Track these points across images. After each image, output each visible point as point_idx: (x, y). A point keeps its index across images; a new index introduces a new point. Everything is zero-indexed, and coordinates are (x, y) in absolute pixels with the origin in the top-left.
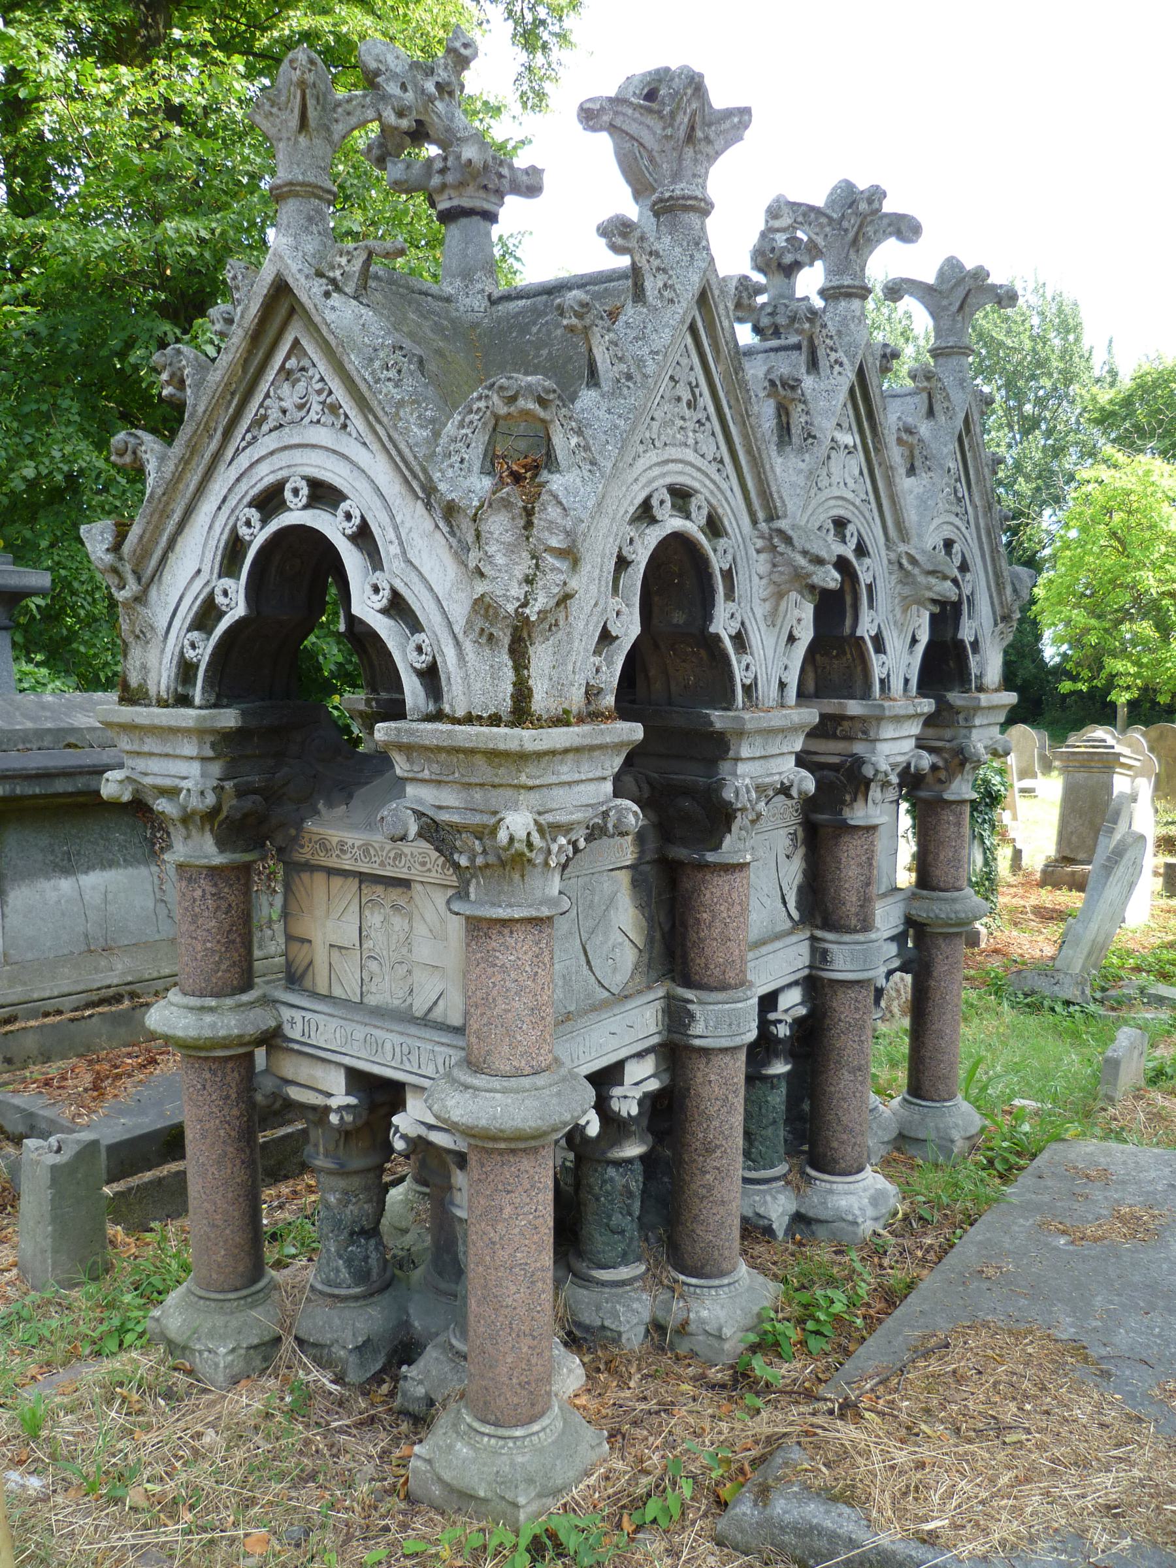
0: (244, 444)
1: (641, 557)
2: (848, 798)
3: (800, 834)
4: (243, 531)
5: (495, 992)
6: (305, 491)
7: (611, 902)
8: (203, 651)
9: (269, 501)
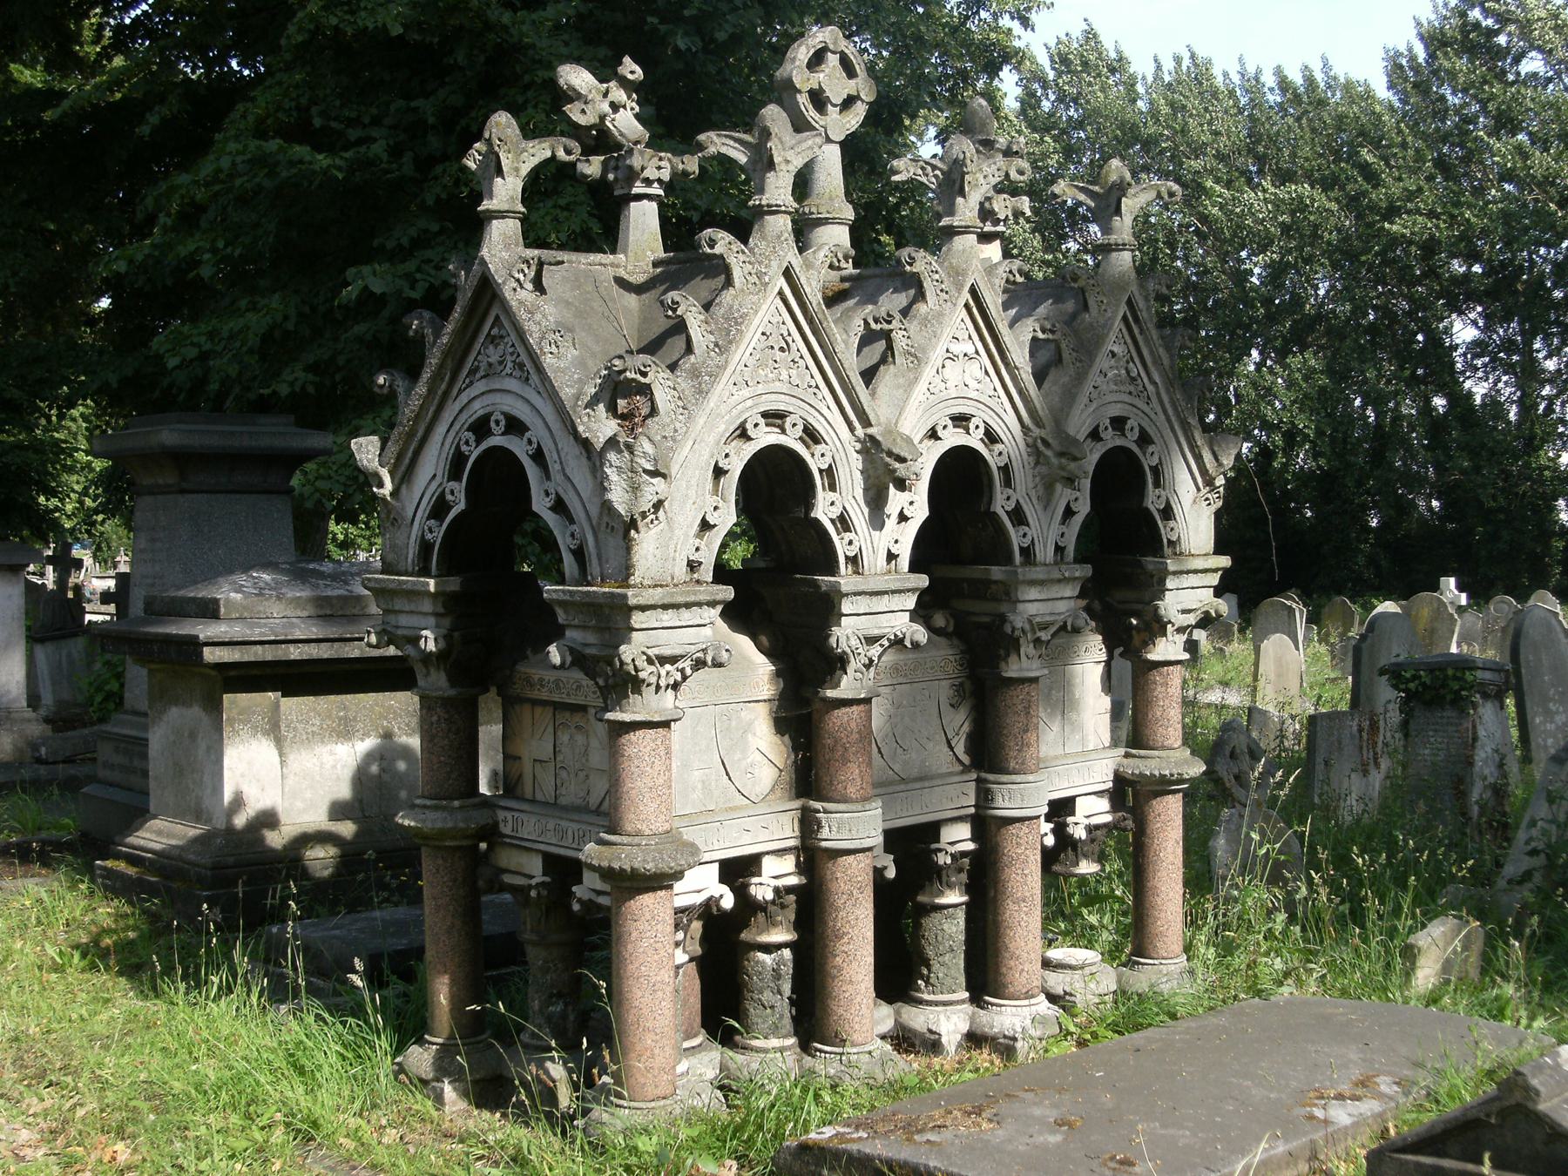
1: (736, 467)
2: (1002, 652)
3: (968, 686)
4: (464, 448)
6: (503, 423)
7: (748, 728)
8: (438, 534)
9: (481, 428)
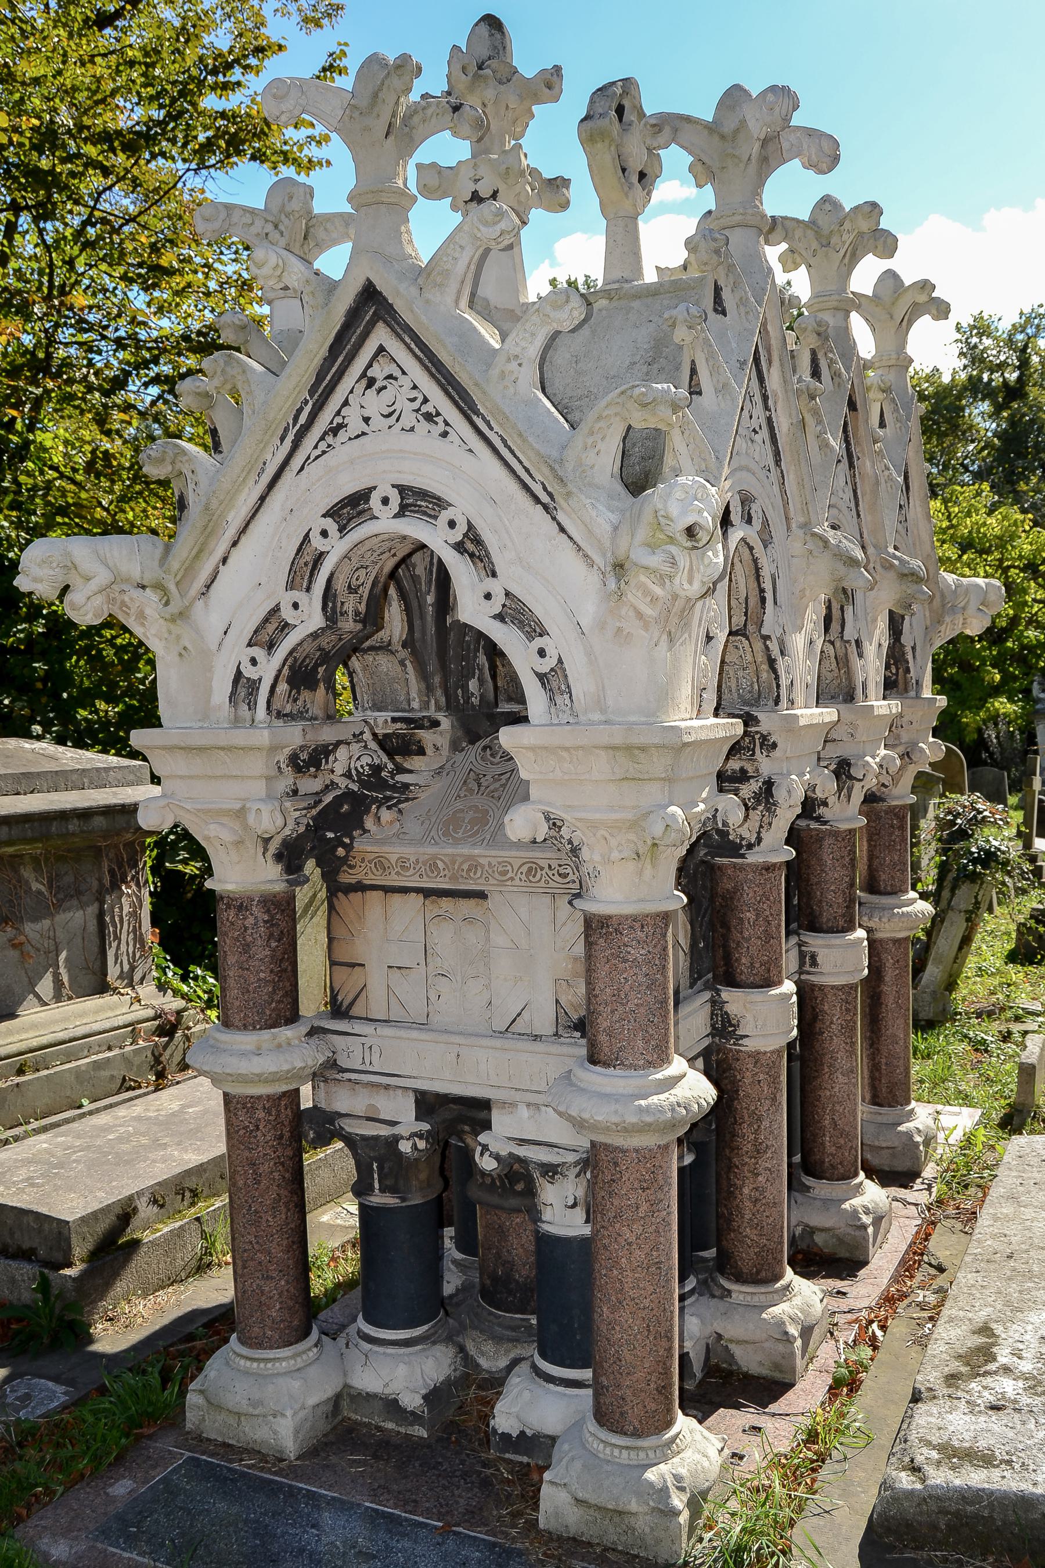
0: (318, 452)
5: (627, 987)
9: (351, 508)
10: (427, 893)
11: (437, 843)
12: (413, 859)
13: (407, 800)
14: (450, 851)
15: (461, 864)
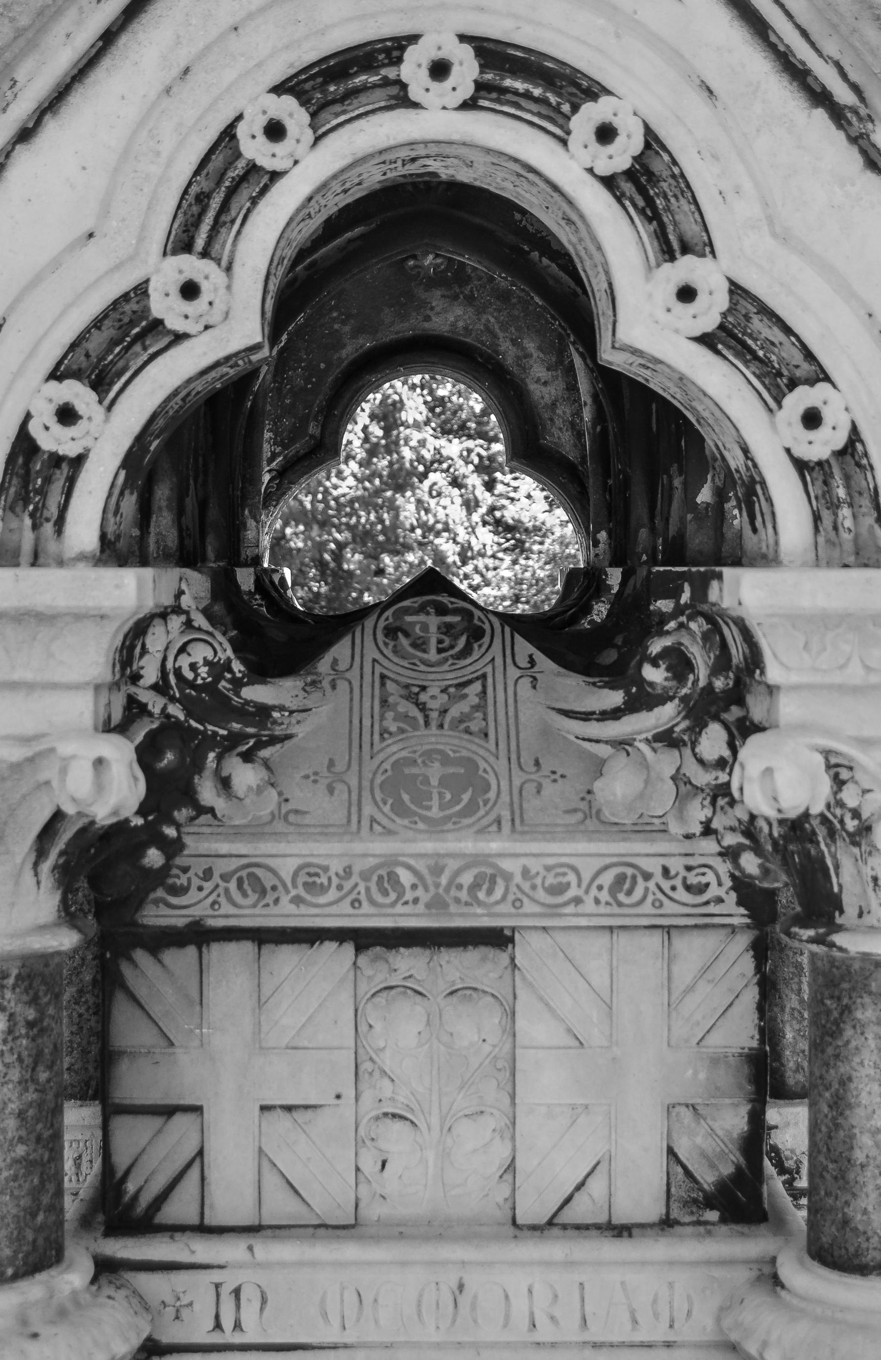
10: (363, 940)
11: (389, 832)
12: (336, 866)
13: (274, 740)
14: (428, 846)
15: (458, 873)
